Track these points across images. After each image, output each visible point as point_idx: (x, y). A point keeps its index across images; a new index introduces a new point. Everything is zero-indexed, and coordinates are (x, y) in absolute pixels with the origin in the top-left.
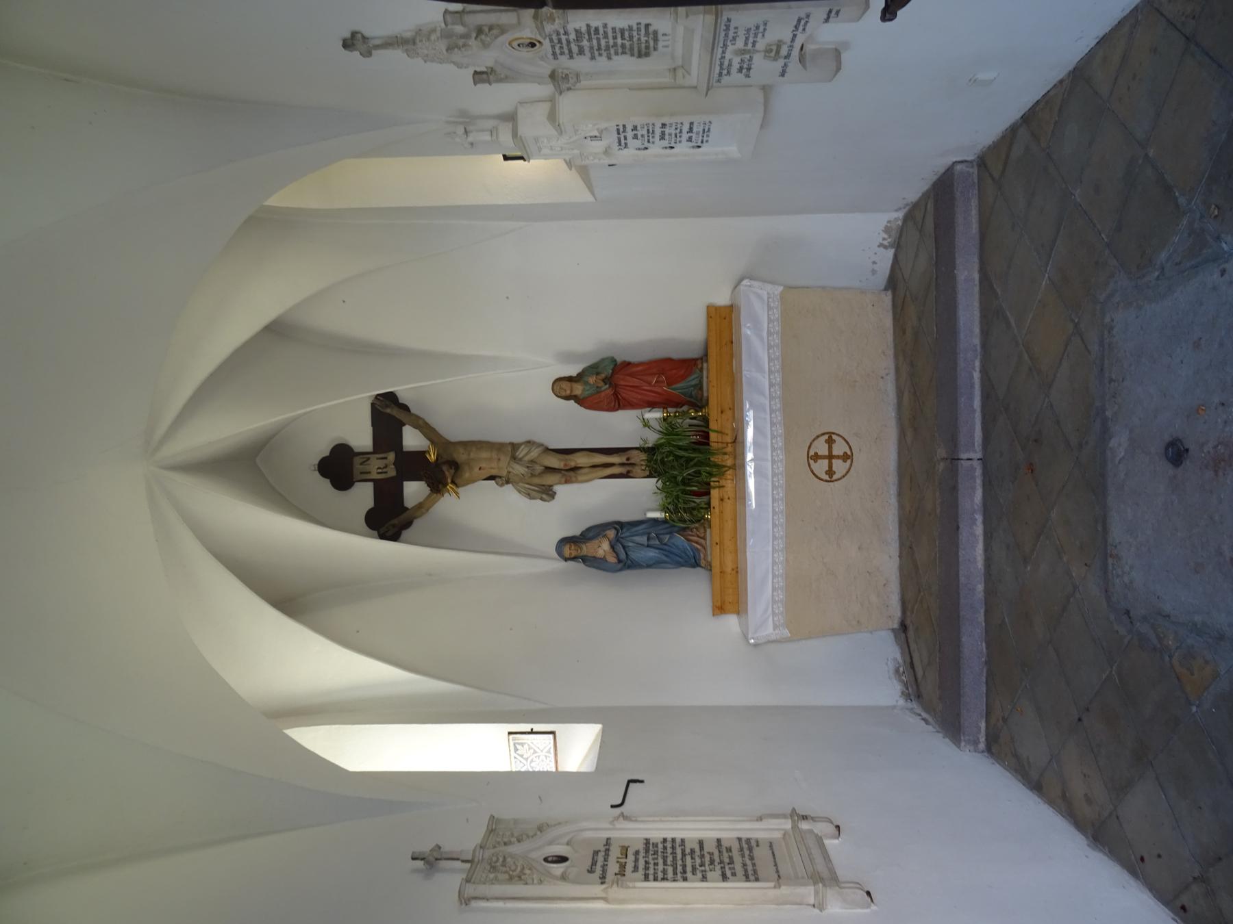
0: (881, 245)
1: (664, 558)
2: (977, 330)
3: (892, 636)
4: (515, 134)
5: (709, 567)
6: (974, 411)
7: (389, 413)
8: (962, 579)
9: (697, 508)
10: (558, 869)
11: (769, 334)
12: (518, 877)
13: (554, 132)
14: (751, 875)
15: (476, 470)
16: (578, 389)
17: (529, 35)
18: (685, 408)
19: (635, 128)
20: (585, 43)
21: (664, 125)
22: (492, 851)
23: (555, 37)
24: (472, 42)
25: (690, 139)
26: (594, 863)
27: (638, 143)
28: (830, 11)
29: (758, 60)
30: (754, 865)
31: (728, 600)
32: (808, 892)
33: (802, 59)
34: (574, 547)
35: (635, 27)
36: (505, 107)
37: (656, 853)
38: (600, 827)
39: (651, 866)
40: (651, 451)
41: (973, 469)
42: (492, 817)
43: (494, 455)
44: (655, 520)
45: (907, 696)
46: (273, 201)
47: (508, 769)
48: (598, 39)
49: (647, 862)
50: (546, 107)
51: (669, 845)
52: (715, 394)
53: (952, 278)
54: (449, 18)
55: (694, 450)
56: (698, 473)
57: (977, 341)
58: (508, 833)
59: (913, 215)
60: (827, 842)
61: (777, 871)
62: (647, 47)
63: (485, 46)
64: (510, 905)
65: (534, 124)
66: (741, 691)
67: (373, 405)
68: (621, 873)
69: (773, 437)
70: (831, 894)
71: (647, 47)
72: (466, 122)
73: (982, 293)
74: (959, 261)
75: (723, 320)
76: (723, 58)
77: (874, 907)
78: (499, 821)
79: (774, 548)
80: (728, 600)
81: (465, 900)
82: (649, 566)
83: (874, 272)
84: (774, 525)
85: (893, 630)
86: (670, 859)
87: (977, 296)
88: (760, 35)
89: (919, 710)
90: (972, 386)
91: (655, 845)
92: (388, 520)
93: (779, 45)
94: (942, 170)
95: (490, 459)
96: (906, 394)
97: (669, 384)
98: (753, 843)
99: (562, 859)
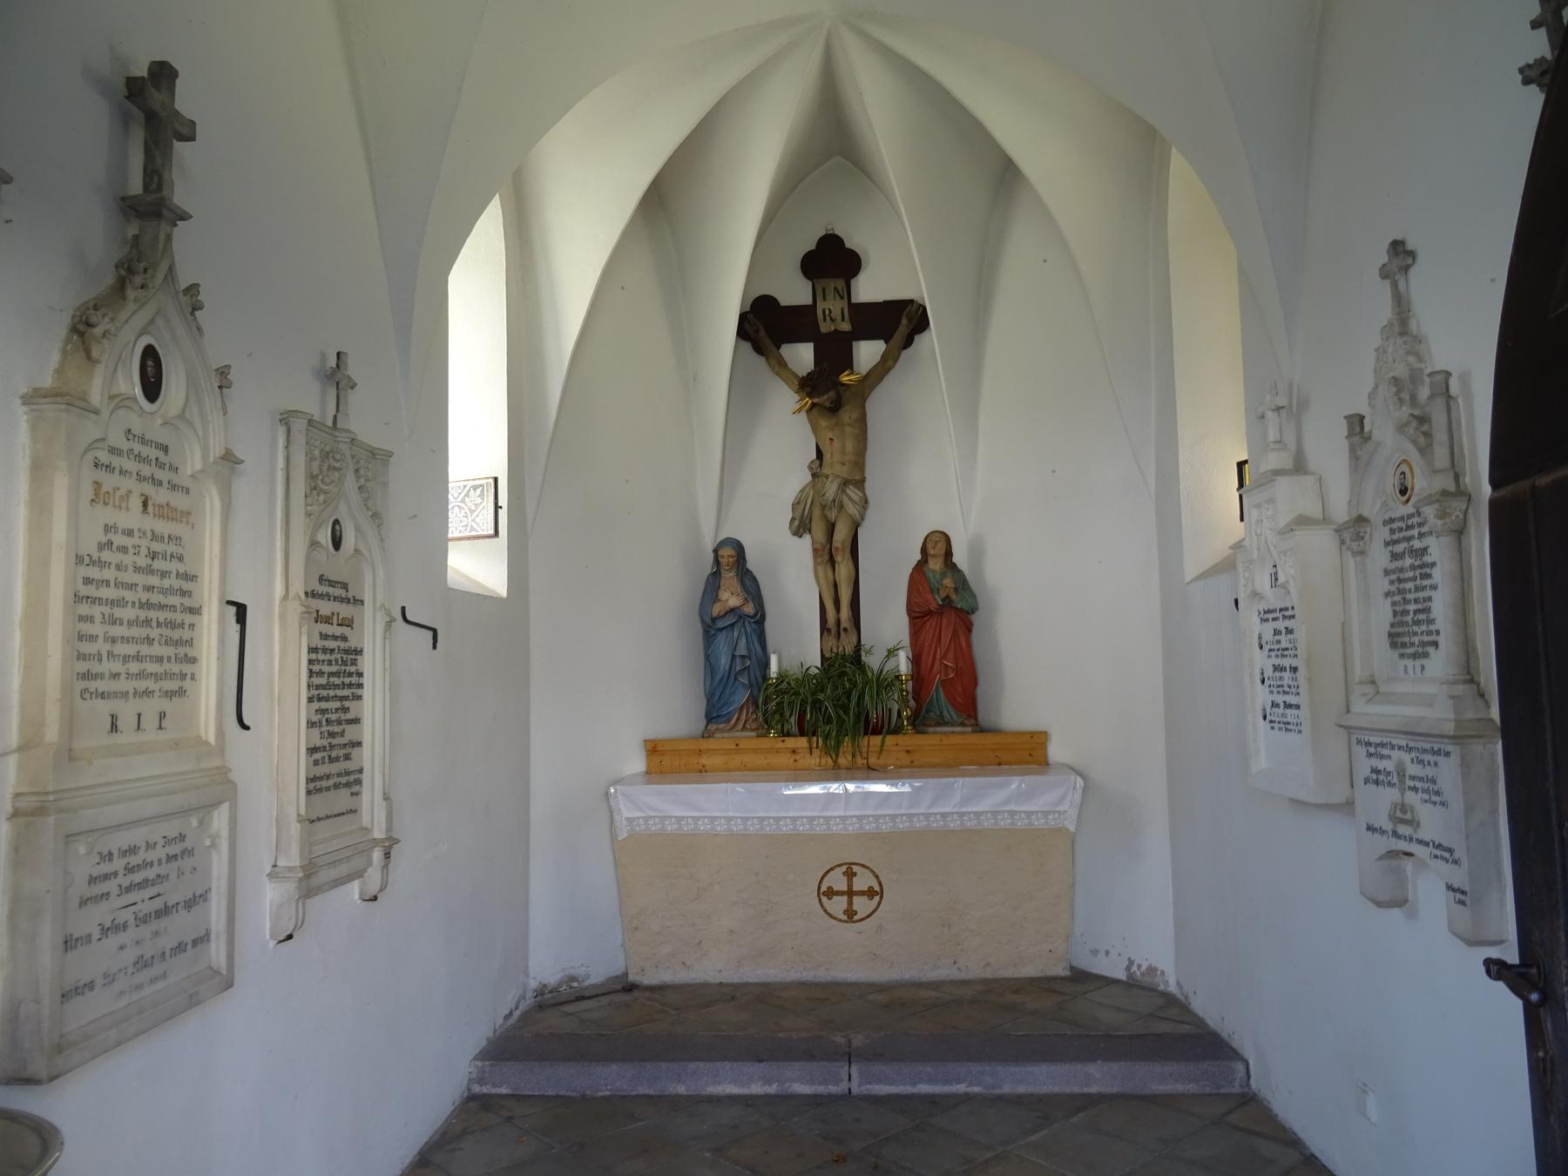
0: (1131, 962)
1: (718, 677)
2: (1021, 1089)
3: (618, 973)
4: (1277, 473)
5: (706, 735)
6: (914, 1084)
7: (900, 322)
8: (692, 1066)
9: (783, 720)
10: (325, 537)
11: (1012, 813)
12: (315, 484)
13: (1282, 525)
14: (315, 786)
15: (830, 435)
16: (935, 565)
17: (1417, 487)
18: (912, 703)
19: (1289, 631)
20: (1408, 561)
21: (1295, 670)
22: (348, 454)
23: (1416, 520)
24: (1406, 410)
25: (1275, 705)
26: (332, 583)
27: (1268, 635)
28: (1463, 892)
29: (1390, 795)
30: (328, 789)
31: (664, 760)
32: (292, 858)
33: (1392, 854)
34: (731, 561)
35: (1432, 627)
36: (1314, 457)
37: (344, 663)
38: (377, 594)
39: (328, 657)
40: (856, 658)
41: (837, 1082)
42: (391, 454)
43: (849, 458)
44: (767, 665)
45: (541, 991)
46: (1178, 165)
47: (451, 478)
48: (1415, 579)
49: (332, 651)
50: (1314, 510)
51: (354, 680)
52: (930, 740)
53: (1091, 1057)
54: (1439, 378)
55: (858, 716)
56: (829, 721)
57: (1007, 1089)
58: (370, 474)
59: (1173, 1005)
60: (356, 884)
61: (319, 819)
62: (1404, 645)
63: (1401, 428)
64: (280, 476)
65: (1292, 497)
66: (549, 776)
67: (912, 301)
68: (319, 618)
69: (877, 818)
70: (290, 887)
71: (1404, 645)
72: (1293, 409)
73: (1072, 1097)
74: (1115, 1066)
75: (1029, 752)
76: (1393, 748)
77: (272, 943)
78: (385, 463)
79: (731, 819)
80: (664, 760)
81: (286, 418)
82: (707, 657)
83: (1095, 952)
84: (761, 819)
85: (626, 974)
86: (337, 681)
87: (1067, 1090)
88: (1426, 797)
89: (523, 1007)
90: (947, 1082)
91: (354, 662)
92: (764, 325)
93: (1414, 823)
94: (1236, 1045)
95: (843, 452)
96: (933, 994)
97: (943, 683)
98: (355, 789)
99: (337, 543)
